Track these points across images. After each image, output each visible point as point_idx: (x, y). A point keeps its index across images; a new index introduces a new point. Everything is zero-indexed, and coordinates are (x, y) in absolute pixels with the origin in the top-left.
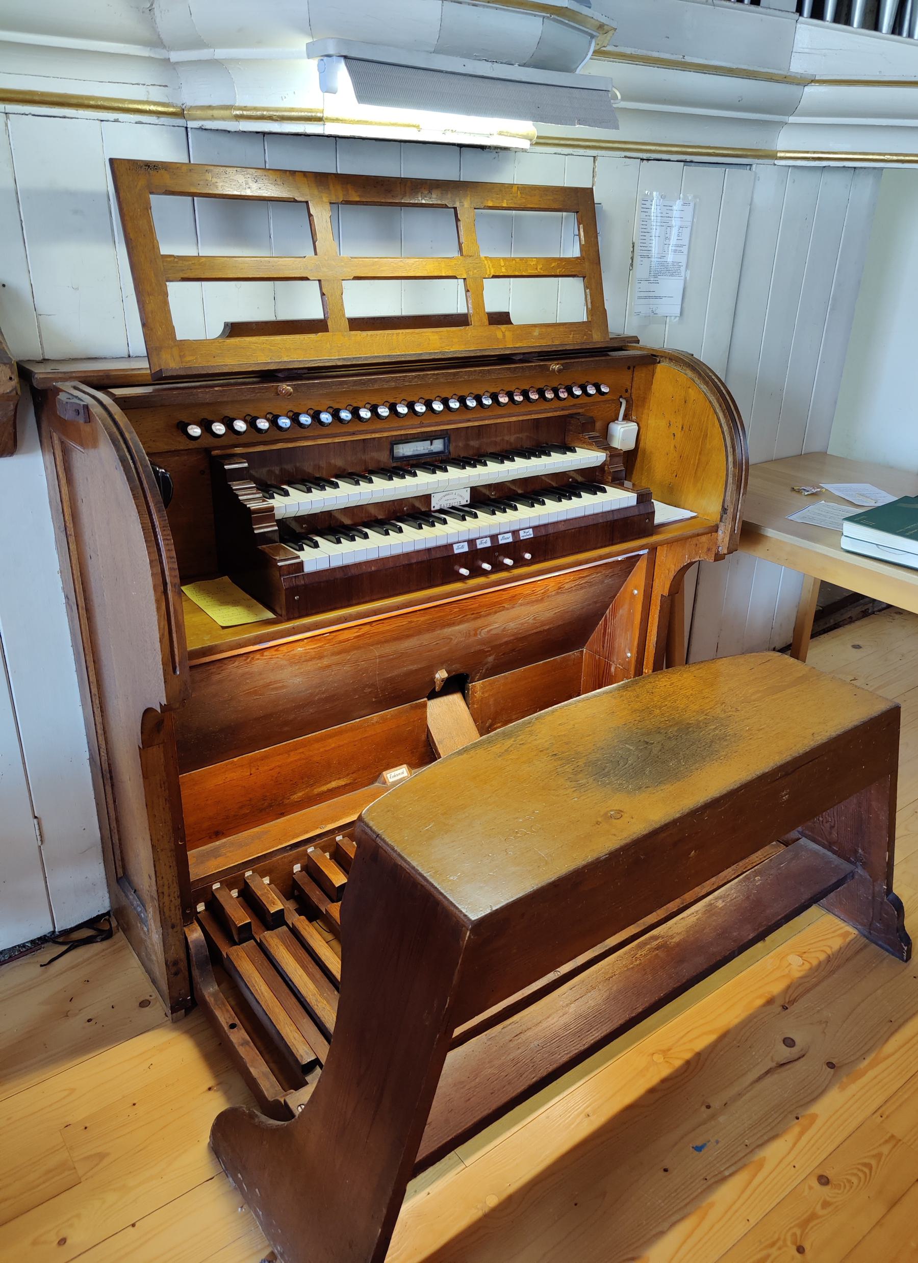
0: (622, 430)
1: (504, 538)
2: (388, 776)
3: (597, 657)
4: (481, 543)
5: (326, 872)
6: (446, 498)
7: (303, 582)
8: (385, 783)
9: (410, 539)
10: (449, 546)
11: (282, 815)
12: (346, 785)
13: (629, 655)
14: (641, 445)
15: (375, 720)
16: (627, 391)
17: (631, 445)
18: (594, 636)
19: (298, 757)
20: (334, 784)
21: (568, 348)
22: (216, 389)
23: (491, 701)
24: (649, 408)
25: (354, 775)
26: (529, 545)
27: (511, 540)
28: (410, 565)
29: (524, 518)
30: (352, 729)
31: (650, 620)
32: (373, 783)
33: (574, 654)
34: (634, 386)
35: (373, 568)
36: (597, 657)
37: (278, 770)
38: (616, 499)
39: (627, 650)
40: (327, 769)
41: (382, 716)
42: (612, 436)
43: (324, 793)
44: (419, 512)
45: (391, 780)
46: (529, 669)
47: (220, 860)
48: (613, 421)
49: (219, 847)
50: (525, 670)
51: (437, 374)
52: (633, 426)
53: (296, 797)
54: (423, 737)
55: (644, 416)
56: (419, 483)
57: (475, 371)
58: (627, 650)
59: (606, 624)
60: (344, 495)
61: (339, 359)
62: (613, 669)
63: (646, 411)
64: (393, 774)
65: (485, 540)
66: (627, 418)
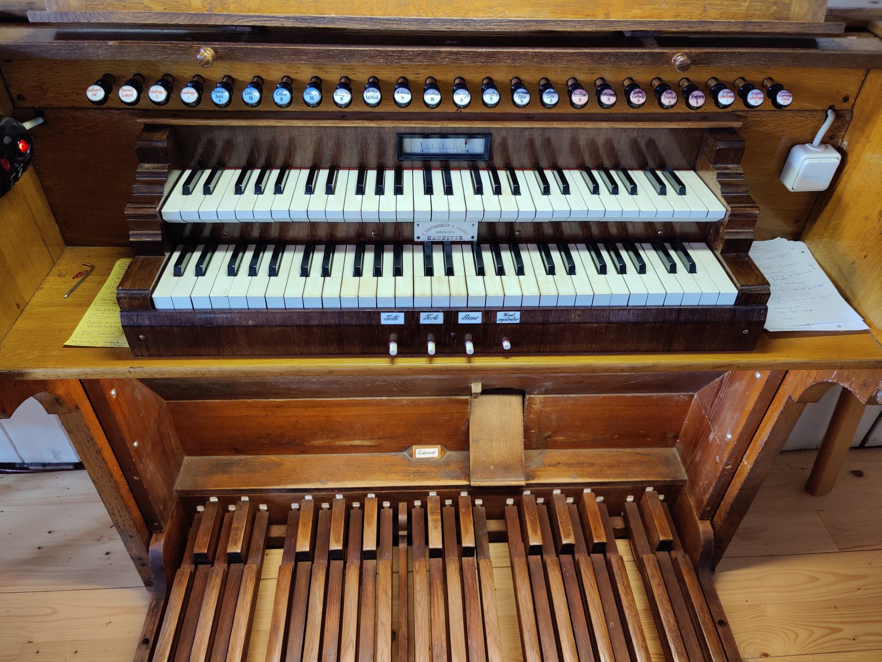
0: (807, 162)
1: (466, 317)
2: (417, 451)
3: (703, 412)
4: (428, 318)
5: (299, 531)
6: (438, 229)
7: (147, 322)
8: (411, 456)
9: (343, 285)
10: (374, 314)
11: (303, 452)
12: (370, 446)
13: (729, 436)
14: (840, 187)
15: (405, 402)
16: (846, 99)
17: (823, 184)
18: (706, 388)
19: (317, 413)
20: (357, 442)
21: (714, 28)
22: (111, 43)
23: (554, 416)
24: (868, 138)
25: (380, 441)
26: (508, 330)
27: (479, 321)
28: (308, 327)
29: (531, 283)
30: (378, 404)
31: (768, 413)
32: (401, 451)
33: (682, 395)
34: (862, 95)
35: (250, 323)
36: (703, 412)
37: (296, 419)
38: (707, 282)
39: (729, 430)
40: (349, 431)
41: (414, 401)
42: (790, 165)
43: (346, 447)
44: (385, 240)
45: (418, 456)
46: (610, 398)
47: (225, 477)
48: (802, 142)
49: (232, 463)
50: (604, 398)
51: (457, 53)
52: (834, 158)
53: (318, 442)
54: (463, 428)
55: (859, 147)
56: (405, 201)
57: (526, 54)
58: (729, 430)
59: (720, 385)
60: (292, 200)
61: (288, 18)
62: (711, 436)
63: (863, 140)
64: (423, 450)
65: (435, 314)
66: (830, 141)
